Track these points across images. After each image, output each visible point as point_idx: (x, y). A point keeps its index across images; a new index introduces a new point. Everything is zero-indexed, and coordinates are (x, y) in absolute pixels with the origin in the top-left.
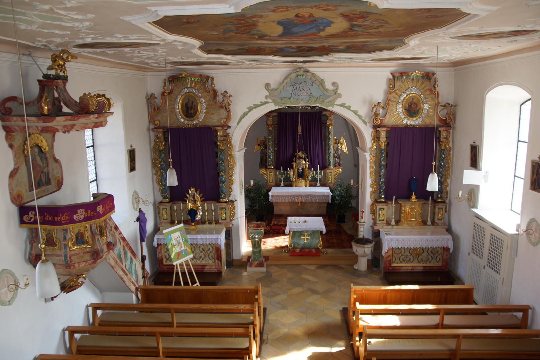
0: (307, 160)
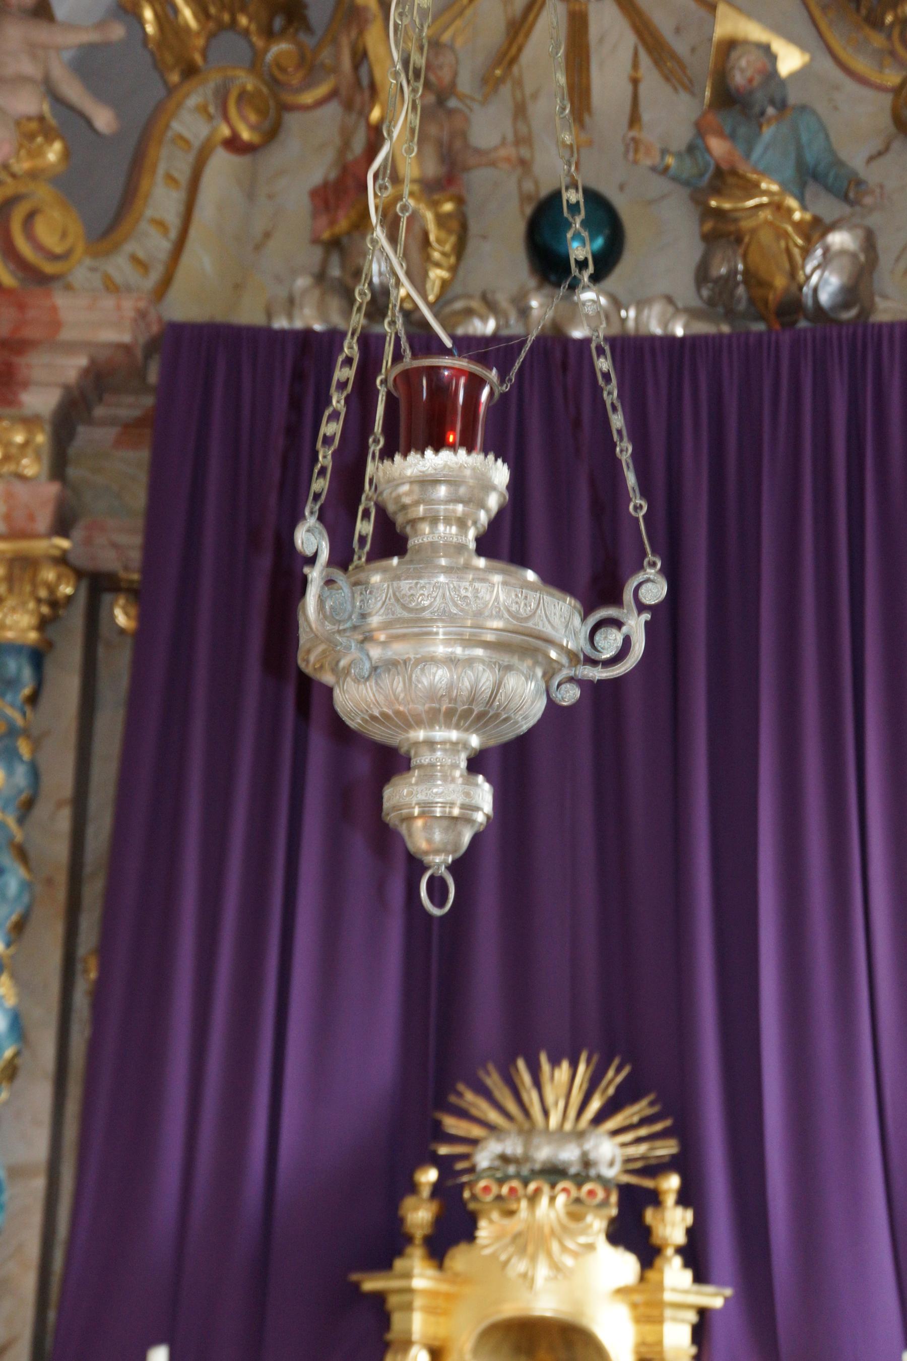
0: (673, 1224)
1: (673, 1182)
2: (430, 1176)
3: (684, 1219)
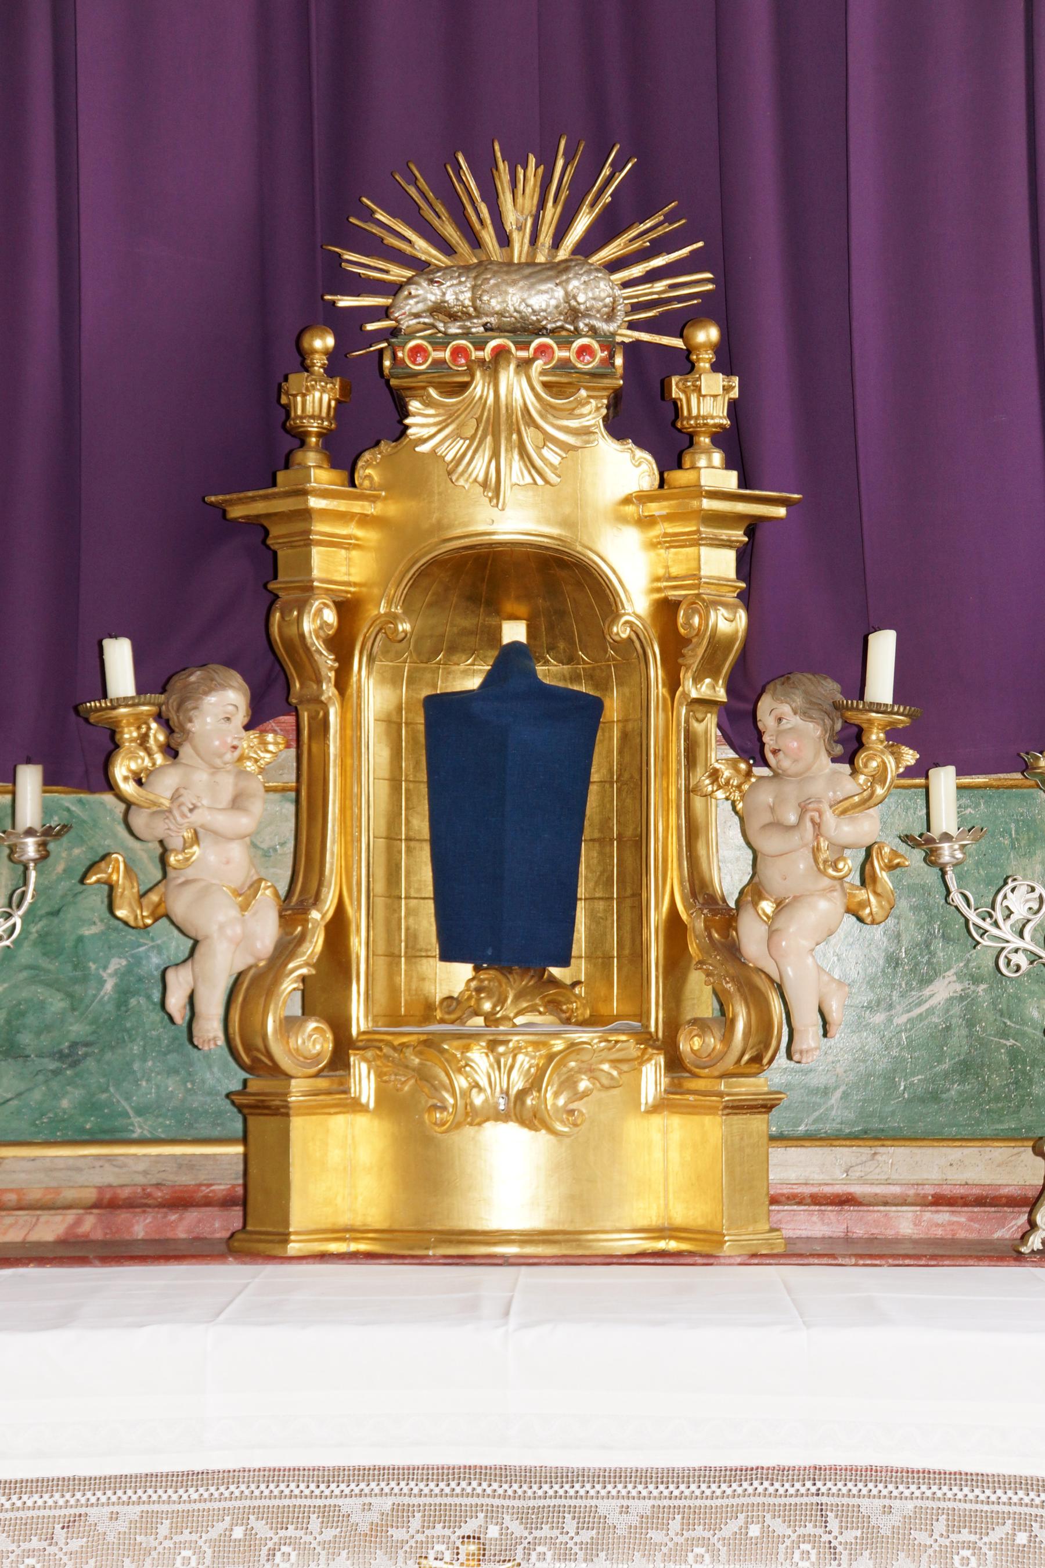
0: (708, 398)
1: (708, 335)
2: (323, 342)
3: (727, 389)
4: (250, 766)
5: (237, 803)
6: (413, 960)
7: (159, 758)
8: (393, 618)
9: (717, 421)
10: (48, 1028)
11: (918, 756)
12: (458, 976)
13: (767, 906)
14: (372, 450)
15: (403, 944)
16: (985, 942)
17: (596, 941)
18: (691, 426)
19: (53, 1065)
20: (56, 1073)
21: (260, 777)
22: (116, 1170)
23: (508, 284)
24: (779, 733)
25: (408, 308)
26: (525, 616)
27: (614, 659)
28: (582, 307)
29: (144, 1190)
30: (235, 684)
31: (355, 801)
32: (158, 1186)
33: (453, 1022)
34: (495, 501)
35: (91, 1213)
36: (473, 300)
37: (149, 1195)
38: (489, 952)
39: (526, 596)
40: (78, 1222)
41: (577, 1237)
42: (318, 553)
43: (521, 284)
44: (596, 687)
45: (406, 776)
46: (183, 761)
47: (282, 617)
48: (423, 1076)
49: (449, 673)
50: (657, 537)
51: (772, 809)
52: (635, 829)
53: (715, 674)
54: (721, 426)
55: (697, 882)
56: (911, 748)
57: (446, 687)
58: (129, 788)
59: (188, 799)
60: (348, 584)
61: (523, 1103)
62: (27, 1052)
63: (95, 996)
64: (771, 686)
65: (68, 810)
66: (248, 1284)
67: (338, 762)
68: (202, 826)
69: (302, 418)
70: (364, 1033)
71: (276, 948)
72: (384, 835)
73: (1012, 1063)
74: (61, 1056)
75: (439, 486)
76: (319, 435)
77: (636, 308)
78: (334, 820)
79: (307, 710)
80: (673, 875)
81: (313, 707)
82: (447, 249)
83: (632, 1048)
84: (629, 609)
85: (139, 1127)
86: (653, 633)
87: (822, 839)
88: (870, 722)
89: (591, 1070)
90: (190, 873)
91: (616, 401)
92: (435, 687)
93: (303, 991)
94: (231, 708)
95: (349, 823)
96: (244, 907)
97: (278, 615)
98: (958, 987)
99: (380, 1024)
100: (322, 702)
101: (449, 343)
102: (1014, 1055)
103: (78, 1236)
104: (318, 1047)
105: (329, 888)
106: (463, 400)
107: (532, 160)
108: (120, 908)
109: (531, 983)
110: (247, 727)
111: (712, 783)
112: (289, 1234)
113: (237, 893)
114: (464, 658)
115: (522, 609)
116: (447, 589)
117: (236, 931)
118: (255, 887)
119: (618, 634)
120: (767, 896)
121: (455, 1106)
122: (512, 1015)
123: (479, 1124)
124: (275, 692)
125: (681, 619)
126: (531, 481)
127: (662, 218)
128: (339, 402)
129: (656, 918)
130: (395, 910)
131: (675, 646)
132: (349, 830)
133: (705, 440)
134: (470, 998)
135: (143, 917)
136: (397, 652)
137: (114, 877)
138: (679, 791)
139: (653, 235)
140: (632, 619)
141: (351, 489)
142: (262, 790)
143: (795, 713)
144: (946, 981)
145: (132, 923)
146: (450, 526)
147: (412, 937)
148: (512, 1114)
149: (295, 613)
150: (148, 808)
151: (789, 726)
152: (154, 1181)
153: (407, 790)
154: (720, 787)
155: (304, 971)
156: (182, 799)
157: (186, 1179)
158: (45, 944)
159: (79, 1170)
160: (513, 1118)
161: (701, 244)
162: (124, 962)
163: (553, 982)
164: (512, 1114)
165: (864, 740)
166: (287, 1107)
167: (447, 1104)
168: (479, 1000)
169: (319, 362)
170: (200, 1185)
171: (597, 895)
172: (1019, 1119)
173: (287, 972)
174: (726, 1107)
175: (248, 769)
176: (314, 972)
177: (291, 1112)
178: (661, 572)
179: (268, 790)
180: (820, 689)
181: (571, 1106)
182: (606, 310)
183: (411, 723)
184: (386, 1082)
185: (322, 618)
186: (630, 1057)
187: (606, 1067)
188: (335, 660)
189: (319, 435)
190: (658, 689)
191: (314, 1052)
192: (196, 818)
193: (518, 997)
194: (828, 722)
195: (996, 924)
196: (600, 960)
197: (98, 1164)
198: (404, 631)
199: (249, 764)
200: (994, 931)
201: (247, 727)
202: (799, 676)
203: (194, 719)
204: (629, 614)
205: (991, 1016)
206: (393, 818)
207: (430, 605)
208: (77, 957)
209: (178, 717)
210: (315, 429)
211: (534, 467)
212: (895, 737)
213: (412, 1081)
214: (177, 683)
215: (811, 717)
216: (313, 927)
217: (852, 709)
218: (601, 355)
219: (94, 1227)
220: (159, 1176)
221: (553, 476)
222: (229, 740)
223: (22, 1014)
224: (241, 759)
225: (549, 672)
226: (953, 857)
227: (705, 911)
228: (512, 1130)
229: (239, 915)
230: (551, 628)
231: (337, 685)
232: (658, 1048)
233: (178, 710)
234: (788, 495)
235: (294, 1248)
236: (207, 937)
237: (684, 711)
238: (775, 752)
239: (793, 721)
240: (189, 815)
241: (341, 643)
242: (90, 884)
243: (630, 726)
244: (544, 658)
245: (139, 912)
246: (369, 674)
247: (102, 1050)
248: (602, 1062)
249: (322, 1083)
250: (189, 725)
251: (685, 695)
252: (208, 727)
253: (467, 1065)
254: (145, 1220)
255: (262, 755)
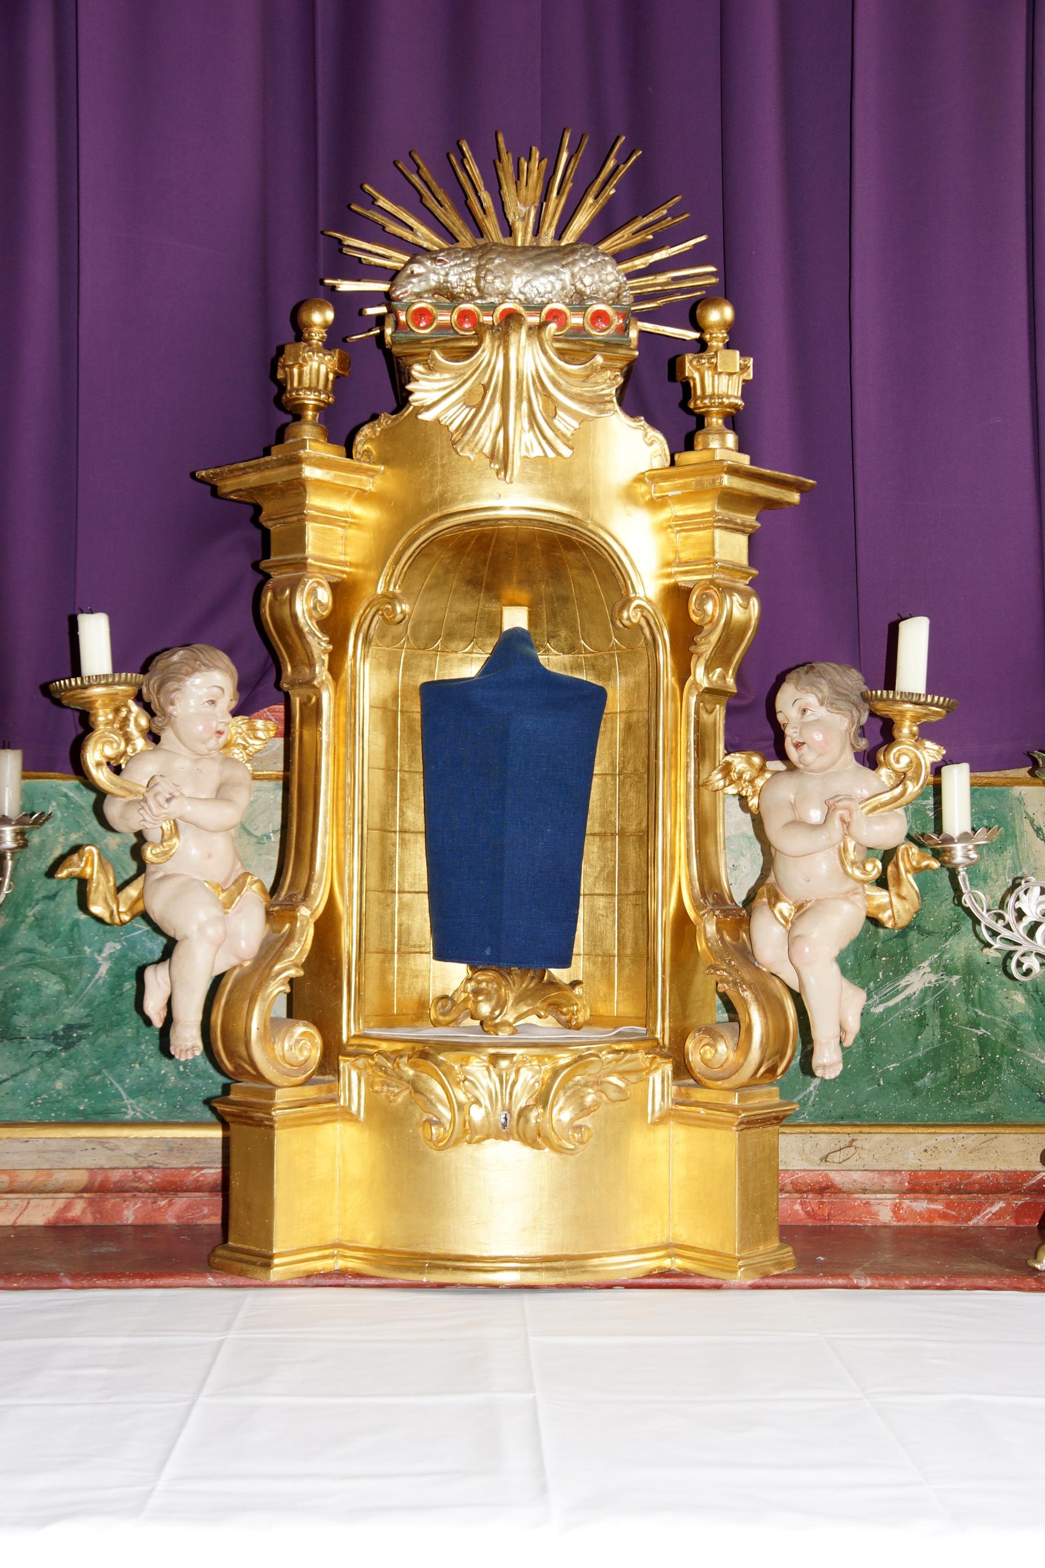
2: (321, 317)
3: (744, 368)
4: (237, 753)
5: (221, 793)
6: (407, 956)
7: (140, 743)
8: (391, 598)
9: (733, 400)
10: (44, 1010)
11: (944, 752)
12: (454, 975)
13: (785, 907)
14: (371, 424)
15: (396, 941)
16: (997, 944)
17: (595, 939)
18: (706, 406)
19: (48, 1048)
20: (50, 1054)
21: (248, 765)
22: (109, 1152)
23: (513, 265)
24: (804, 725)
25: (410, 286)
26: (527, 603)
27: (619, 648)
28: (588, 292)
29: (135, 1173)
30: (221, 665)
31: (347, 792)
32: (149, 1169)
33: (447, 1024)
34: (503, 473)
35: (82, 1197)
36: (477, 280)
37: (140, 1178)
38: (488, 952)
39: (528, 581)
40: (68, 1207)
41: (581, 1262)
42: (313, 529)
43: (527, 265)
44: (598, 676)
45: (402, 765)
46: (165, 747)
47: (275, 596)
48: (416, 1088)
49: (446, 661)
50: (668, 520)
51: (793, 806)
52: (640, 823)
53: (726, 663)
54: (735, 406)
55: (706, 881)
56: (938, 743)
57: (444, 675)
58: (102, 776)
59: (164, 788)
60: (344, 563)
61: (527, 1121)
62: (23, 1035)
63: (90, 979)
64: (793, 675)
65: (66, 796)
66: (222, 1342)
67: (331, 749)
68: (181, 818)
69: (298, 390)
70: (355, 1037)
71: (261, 947)
72: (378, 826)
73: (982, 1050)
74: (56, 1038)
75: (442, 458)
76: (317, 408)
77: (640, 298)
78: (326, 812)
79: (299, 695)
80: (681, 871)
81: (305, 691)
82: (451, 237)
83: (642, 1057)
84: (640, 592)
85: (132, 1108)
86: (663, 620)
87: (848, 839)
88: (902, 713)
89: (597, 1083)
90: (169, 867)
91: (630, 373)
92: (432, 673)
93: (290, 996)
94: (216, 690)
95: (341, 815)
96: (227, 905)
97: (269, 594)
98: (933, 978)
99: (371, 1024)
100: (314, 686)
101: (455, 307)
102: (983, 1041)
103: (69, 1221)
104: (306, 1053)
105: (320, 883)
106: (471, 363)
107: (536, 154)
108: (95, 904)
109: (532, 985)
110: (235, 713)
111: (724, 778)
112: (271, 1257)
113: (220, 888)
114: (462, 645)
115: (524, 595)
116: (447, 571)
117: (216, 929)
118: (240, 883)
119: (629, 619)
120: (785, 897)
121: (453, 1121)
122: (511, 1020)
123: (478, 1142)
124: (268, 680)
125: (692, 607)
126: (542, 454)
127: (665, 212)
128: (337, 376)
129: (664, 915)
130: (388, 905)
131: (686, 636)
132: (341, 822)
133: (716, 421)
134: (466, 1000)
135: (119, 913)
136: (393, 637)
137: (88, 870)
138: (688, 785)
139: (656, 228)
140: (644, 604)
141: (348, 460)
142: (249, 777)
143: (822, 704)
144: (922, 972)
145: (108, 920)
146: (453, 501)
147: (405, 933)
148: (514, 1132)
149: (288, 592)
150: (124, 797)
151: (812, 718)
152: (145, 1165)
153: (402, 780)
154: (732, 782)
155: (292, 973)
156: (158, 788)
157: (176, 1162)
158: (41, 927)
159: (71, 1152)
160: (516, 1136)
161: (703, 238)
162: (119, 947)
163: (553, 984)
164: (514, 1132)
165: (895, 733)
166: (271, 1120)
167: (443, 1120)
168: (476, 1003)
169: (317, 335)
170: (192, 1168)
171: (597, 891)
172: (989, 1105)
173: (273, 974)
174: (741, 1123)
175: (236, 756)
176: (301, 973)
177: (276, 1126)
178: (671, 556)
179: (255, 778)
180: (846, 679)
181: (577, 1123)
182: (612, 294)
183: (407, 712)
184: (377, 1092)
185: (316, 597)
186: (639, 1068)
187: (614, 1079)
188: (329, 643)
189: (317, 408)
190: (668, 679)
191: (301, 1058)
192: (174, 808)
193: (519, 1000)
194: (855, 713)
195: (1008, 926)
196: (600, 959)
197: (90, 1146)
198: (402, 612)
199: (236, 751)
200: (1005, 933)
201: (235, 713)
202: (822, 664)
203: (176, 702)
204: (639, 598)
205: (963, 1007)
206: (387, 810)
207: (429, 588)
208: (73, 941)
209: (158, 699)
210: (313, 402)
211: (545, 438)
212: (926, 732)
213: (406, 1093)
214: (160, 663)
215: (839, 709)
216: (302, 926)
217: (881, 699)
218: (617, 322)
219: (84, 1212)
220: (150, 1158)
221: (565, 447)
222: (214, 724)
223: (19, 996)
224: (227, 746)
225: (553, 660)
226: (968, 857)
227: (717, 912)
228: (512, 1150)
229: (220, 914)
230: (553, 615)
231: (330, 669)
232: (666, 1057)
233: (158, 692)
234: (804, 479)
235: (276, 1273)
236: (186, 938)
237: (693, 700)
238: (798, 745)
239: (818, 711)
240: (166, 805)
241: (335, 627)
242: (62, 879)
243: (634, 717)
244: (543, 646)
245: (115, 907)
246: (365, 657)
247: (96, 1033)
248: (609, 1074)
249: (310, 1092)
250: (170, 708)
251: (695, 683)
252: (192, 710)
253: (466, 1079)
254: (135, 1204)
255: (251, 742)
